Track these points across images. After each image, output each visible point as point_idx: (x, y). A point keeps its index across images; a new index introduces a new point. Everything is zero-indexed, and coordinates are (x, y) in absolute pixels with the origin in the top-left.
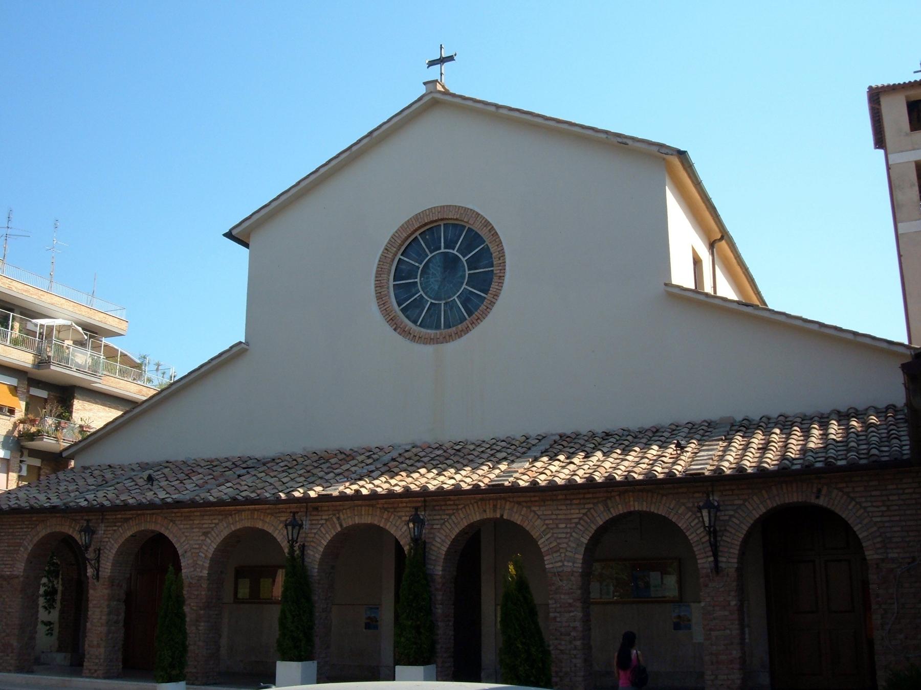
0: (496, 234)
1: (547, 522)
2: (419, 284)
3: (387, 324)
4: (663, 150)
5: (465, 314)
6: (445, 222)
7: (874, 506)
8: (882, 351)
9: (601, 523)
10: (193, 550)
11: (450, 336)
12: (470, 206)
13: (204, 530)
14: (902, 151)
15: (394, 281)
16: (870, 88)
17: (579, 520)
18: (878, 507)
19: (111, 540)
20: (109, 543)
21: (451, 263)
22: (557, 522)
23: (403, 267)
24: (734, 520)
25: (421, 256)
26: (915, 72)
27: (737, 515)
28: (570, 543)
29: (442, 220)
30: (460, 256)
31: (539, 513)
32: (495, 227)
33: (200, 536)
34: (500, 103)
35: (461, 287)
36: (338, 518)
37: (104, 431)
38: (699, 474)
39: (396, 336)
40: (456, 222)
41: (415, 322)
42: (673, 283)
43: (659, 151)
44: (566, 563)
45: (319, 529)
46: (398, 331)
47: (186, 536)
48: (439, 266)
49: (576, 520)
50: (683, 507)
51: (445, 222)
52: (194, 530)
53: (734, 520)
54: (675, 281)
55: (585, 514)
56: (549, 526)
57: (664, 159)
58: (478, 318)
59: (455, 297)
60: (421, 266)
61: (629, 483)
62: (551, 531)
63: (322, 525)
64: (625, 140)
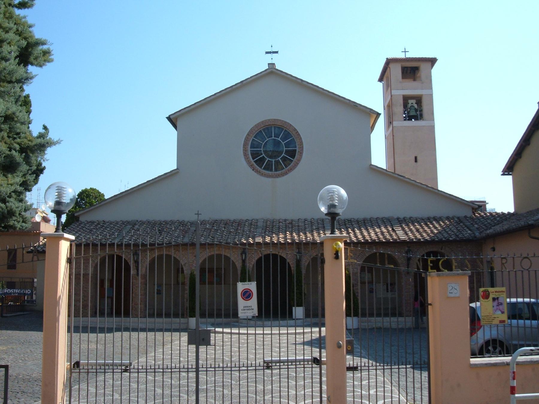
0: (299, 135)
3: (249, 168)
4: (372, 112)
5: (284, 166)
6: (274, 126)
8: (453, 199)
9: (368, 256)
11: (279, 175)
12: (288, 121)
14: (398, 90)
15: (251, 148)
16: (387, 59)
19: (144, 258)
20: (143, 260)
23: (255, 143)
25: (263, 139)
26: (402, 52)
29: (273, 125)
30: (281, 141)
32: (299, 132)
34: (304, 79)
35: (282, 155)
36: (260, 251)
38: (405, 240)
39: (253, 172)
40: (280, 127)
42: (440, 189)
43: (370, 111)
45: (252, 255)
46: (255, 170)
47: (185, 257)
49: (359, 255)
51: (274, 126)
54: (373, 163)
55: (362, 252)
57: (370, 114)
58: (291, 169)
60: (263, 143)
61: (373, 243)
63: (253, 254)
64: (356, 105)
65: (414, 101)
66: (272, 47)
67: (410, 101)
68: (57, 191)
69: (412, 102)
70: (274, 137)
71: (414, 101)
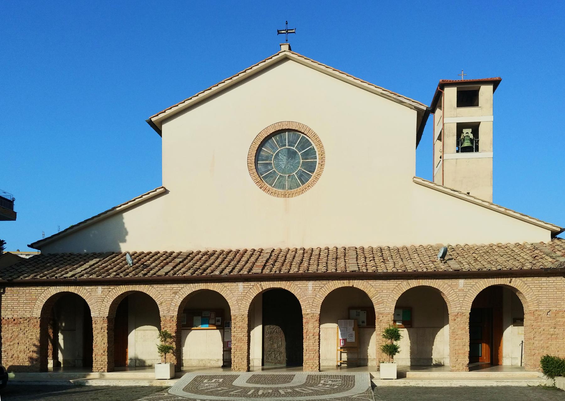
1: (377, 289)
2: (273, 165)
7: (535, 288)
10: (167, 302)
13: (174, 291)
17: (394, 289)
18: (537, 288)
21: (292, 154)
22: (382, 289)
24: (470, 291)
27: (472, 289)
28: (389, 300)
31: (373, 285)
33: (171, 294)
37: (51, 239)
41: (271, 185)
44: (386, 309)
48: (285, 156)
50: (446, 285)
52: (167, 291)
53: (470, 291)
56: (378, 291)
59: (294, 173)
60: (274, 155)
62: (379, 294)
63: (251, 288)
65: (470, 131)
66: (287, 24)
67: (465, 131)
68: (389, 355)
69: (467, 132)
70: (289, 146)
71: (470, 131)
